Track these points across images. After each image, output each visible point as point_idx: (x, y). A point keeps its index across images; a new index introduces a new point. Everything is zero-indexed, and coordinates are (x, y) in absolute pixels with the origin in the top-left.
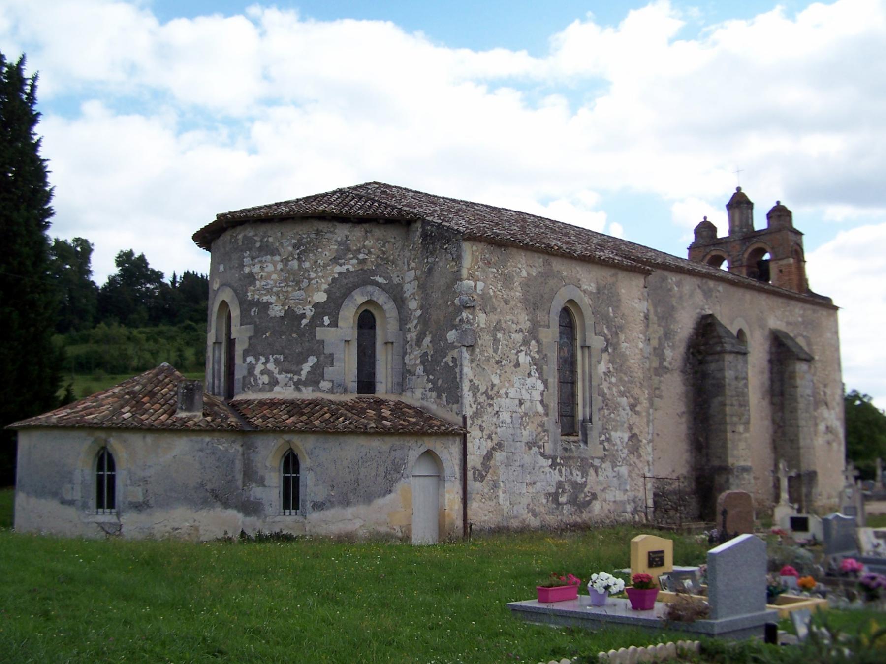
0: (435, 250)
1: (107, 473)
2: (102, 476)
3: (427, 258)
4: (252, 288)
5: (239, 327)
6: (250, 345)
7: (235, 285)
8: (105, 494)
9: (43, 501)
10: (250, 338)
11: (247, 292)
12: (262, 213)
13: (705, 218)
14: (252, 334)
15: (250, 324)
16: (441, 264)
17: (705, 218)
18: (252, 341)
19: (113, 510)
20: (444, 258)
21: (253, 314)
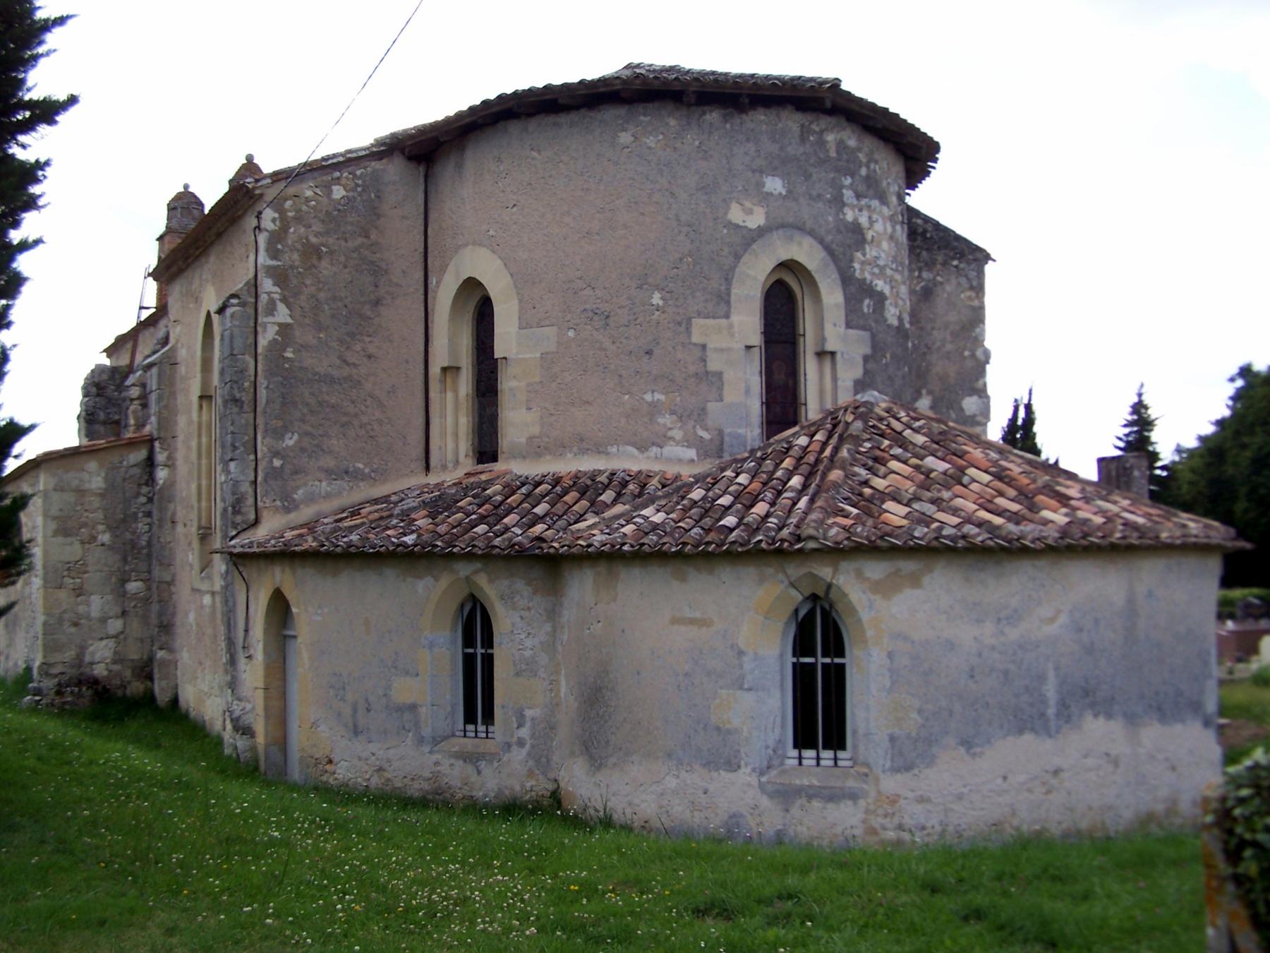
0: (934, 262)
1: (480, 651)
2: (474, 656)
3: (920, 270)
4: (859, 255)
5: (842, 329)
6: (866, 372)
7: (829, 238)
8: (819, 714)
9: (1178, 727)
10: (866, 359)
11: (852, 261)
12: (666, 82)
13: (186, 187)
14: (868, 351)
15: (863, 328)
16: (948, 288)
17: (186, 187)
18: (869, 366)
19: (841, 754)
20: (954, 281)
21: (866, 310)
